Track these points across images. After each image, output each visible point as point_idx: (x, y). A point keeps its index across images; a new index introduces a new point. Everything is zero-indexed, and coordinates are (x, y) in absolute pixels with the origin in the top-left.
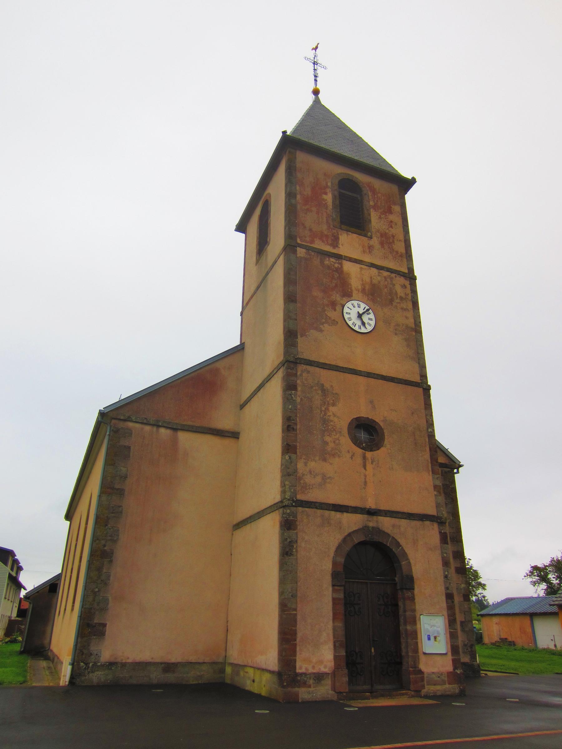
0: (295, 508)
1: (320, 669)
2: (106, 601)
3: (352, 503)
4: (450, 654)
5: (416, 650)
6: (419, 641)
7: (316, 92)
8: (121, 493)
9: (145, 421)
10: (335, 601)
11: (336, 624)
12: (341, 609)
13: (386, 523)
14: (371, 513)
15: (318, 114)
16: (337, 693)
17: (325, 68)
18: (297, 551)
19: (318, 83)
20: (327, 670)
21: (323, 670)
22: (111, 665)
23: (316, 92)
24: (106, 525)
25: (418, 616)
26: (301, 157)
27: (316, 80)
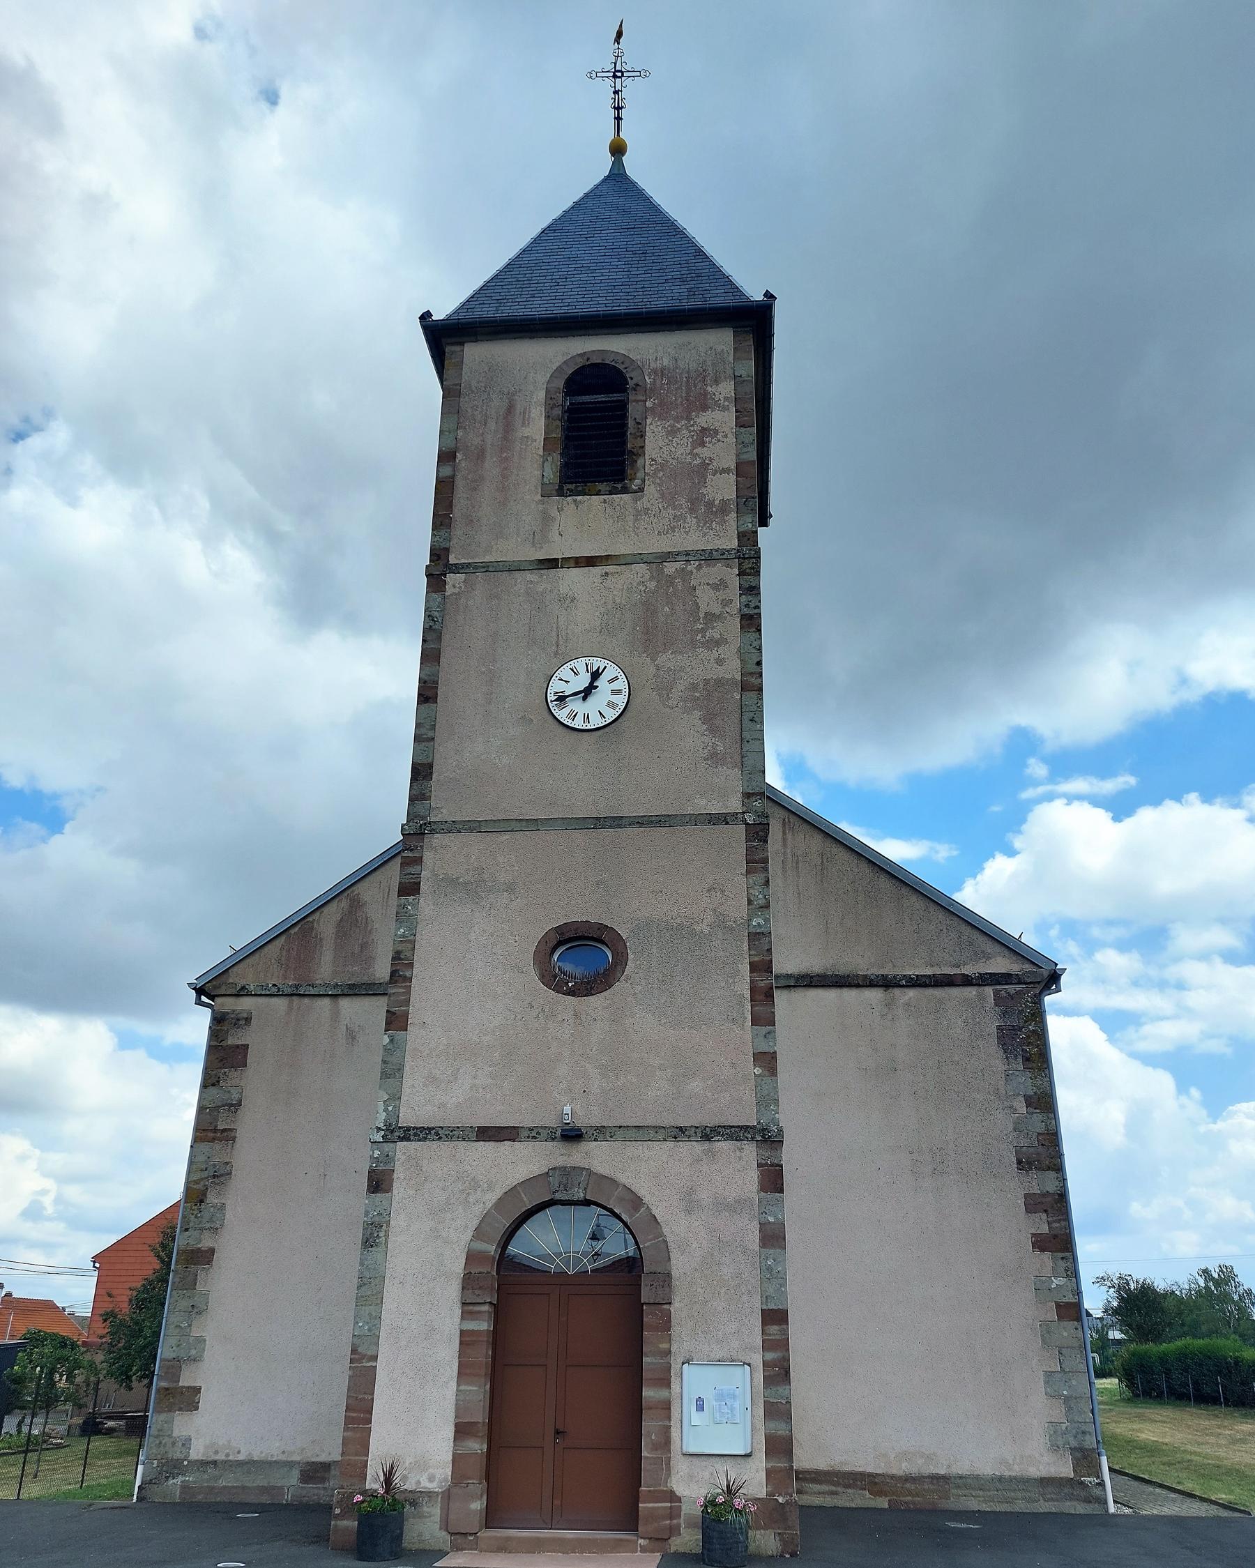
0: (392, 1145)
1: (419, 1482)
2: (201, 1340)
3: (526, 1121)
4: (761, 1455)
5: (665, 1443)
6: (674, 1423)
7: (618, 149)
8: (228, 1136)
9: (274, 990)
10: (467, 1340)
11: (462, 1388)
12: (482, 1355)
13: (596, 1157)
14: (572, 1135)
15: (617, 202)
16: (452, 1534)
17: (643, 74)
18: (387, 1236)
19: (623, 123)
20: (433, 1486)
21: (426, 1484)
22: (203, 1464)
23: (618, 149)
24: (202, 1201)
25: (675, 1367)
26: (475, 354)
27: (618, 119)
